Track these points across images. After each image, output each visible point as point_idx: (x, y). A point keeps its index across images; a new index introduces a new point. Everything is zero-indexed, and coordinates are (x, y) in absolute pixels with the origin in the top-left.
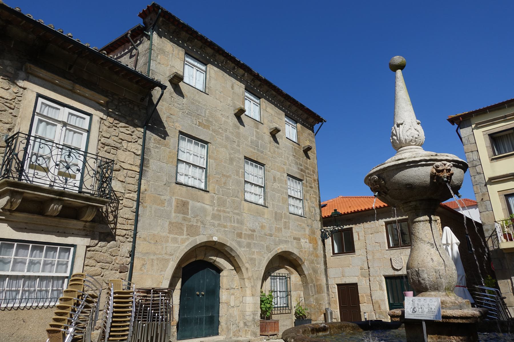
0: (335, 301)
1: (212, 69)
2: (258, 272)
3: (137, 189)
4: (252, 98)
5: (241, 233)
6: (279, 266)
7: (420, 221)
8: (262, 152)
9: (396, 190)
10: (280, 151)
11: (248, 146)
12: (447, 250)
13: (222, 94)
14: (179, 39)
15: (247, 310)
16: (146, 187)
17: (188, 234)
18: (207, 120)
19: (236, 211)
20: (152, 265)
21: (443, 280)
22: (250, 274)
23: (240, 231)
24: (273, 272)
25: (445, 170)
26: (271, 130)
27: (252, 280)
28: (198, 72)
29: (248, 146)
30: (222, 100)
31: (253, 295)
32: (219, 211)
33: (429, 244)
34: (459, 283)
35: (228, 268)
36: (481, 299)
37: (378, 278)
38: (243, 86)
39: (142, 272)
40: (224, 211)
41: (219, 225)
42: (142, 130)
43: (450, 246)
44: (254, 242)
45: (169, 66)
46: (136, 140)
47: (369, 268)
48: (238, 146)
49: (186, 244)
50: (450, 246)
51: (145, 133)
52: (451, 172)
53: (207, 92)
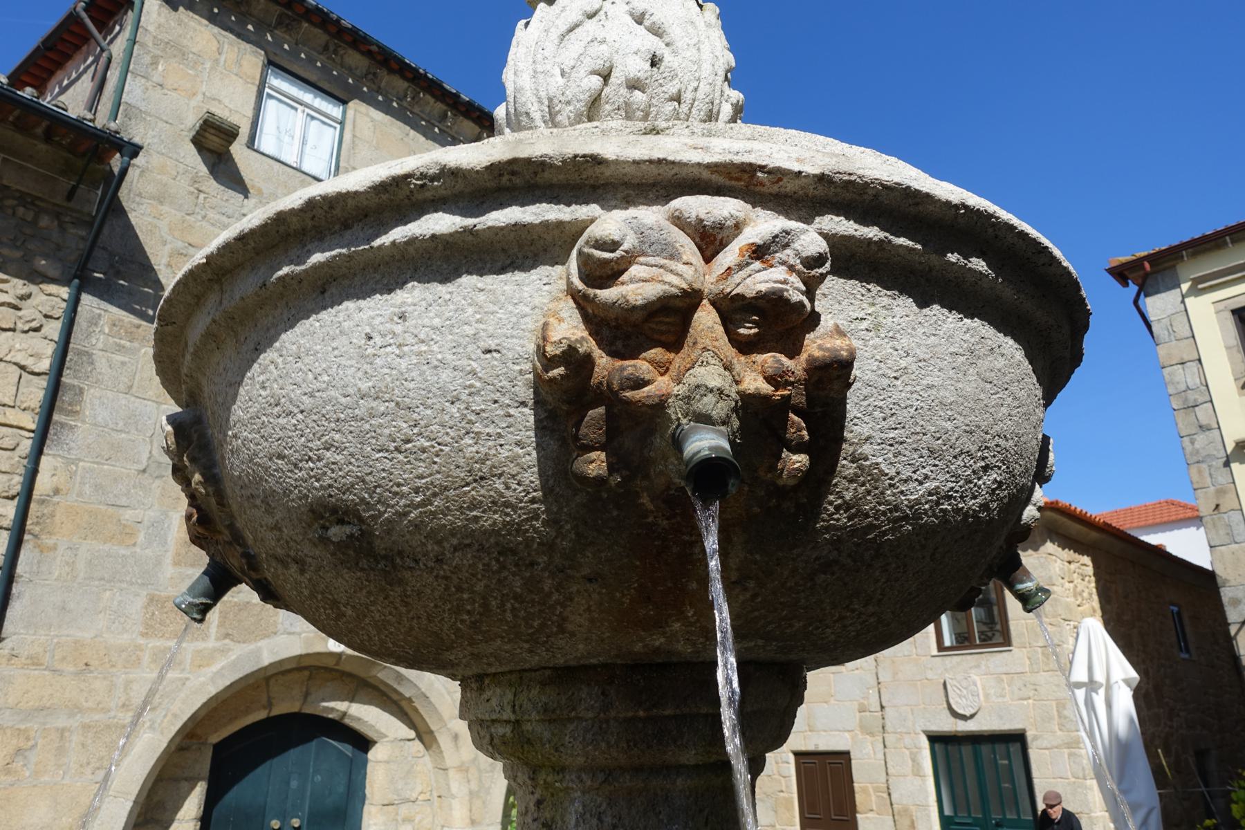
0: (790, 801)
3: (18, 488)
12: (1090, 704)
14: (244, 17)
16: (61, 480)
17: (227, 636)
20: (61, 751)
25: (706, 319)
28: (315, 123)
39: (10, 779)
42: (64, 292)
43: (1102, 691)
45: (200, 97)
46: (34, 324)
47: (882, 707)
49: (215, 668)
50: (1102, 691)
51: (75, 303)
52: (816, 345)
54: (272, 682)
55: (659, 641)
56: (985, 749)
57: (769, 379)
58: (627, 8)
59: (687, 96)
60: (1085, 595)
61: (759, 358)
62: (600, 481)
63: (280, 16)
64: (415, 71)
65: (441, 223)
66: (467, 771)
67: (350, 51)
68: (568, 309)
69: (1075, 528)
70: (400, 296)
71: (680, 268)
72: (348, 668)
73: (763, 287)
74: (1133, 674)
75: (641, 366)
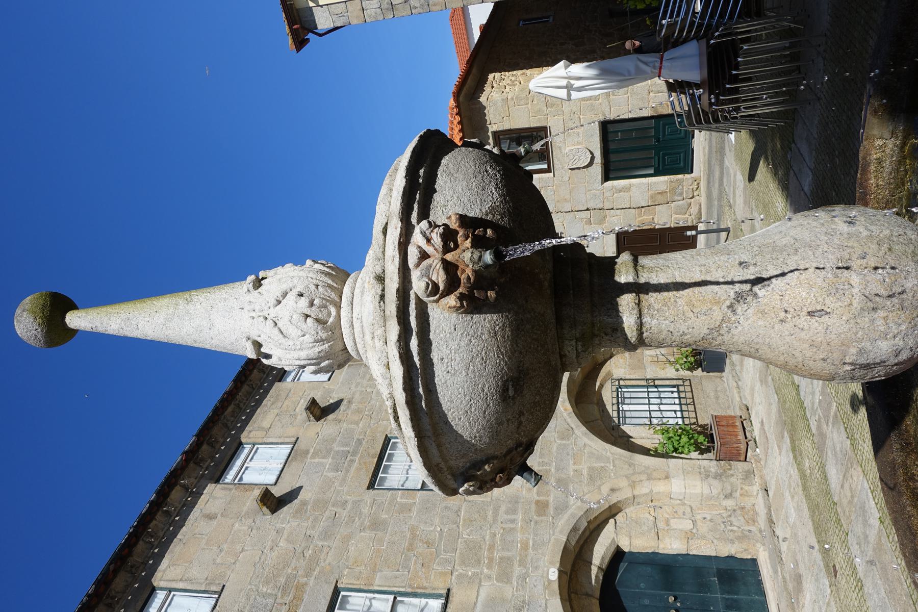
1: (167, 572)
2: (617, 462)
4: (238, 463)
5: (537, 502)
6: (598, 404)
7: (640, 326)
8: (359, 442)
9: (520, 423)
10: (357, 396)
11: (344, 480)
13: (225, 547)
15: (698, 490)
18: (285, 590)
19: (490, 513)
21: (909, 285)
22: (623, 483)
23: (533, 506)
24: (610, 418)
25: (449, 257)
26: (312, 418)
27: (636, 478)
29: (344, 480)
30: (238, 547)
31: (667, 477)
32: (491, 560)
33: (740, 309)
34: (654, 67)
35: (613, 535)
36: (692, 23)
37: (608, 194)
38: (210, 487)
40: (492, 547)
41: (522, 563)
43: (572, 82)
44: (553, 470)
48: (344, 504)
50: (572, 82)
52: (454, 224)
53: (219, 589)
55: (546, 284)
56: (612, 146)
57: (467, 239)
58: (272, 308)
59: (315, 281)
60: (513, 79)
61: (459, 242)
62: (496, 293)
64: (131, 535)
65: (414, 344)
66: (634, 482)
67: (113, 586)
68: (444, 301)
69: (470, 82)
70: (435, 361)
71: (434, 264)
72: (569, 567)
73: (440, 240)
74: (562, 63)
75: (463, 278)
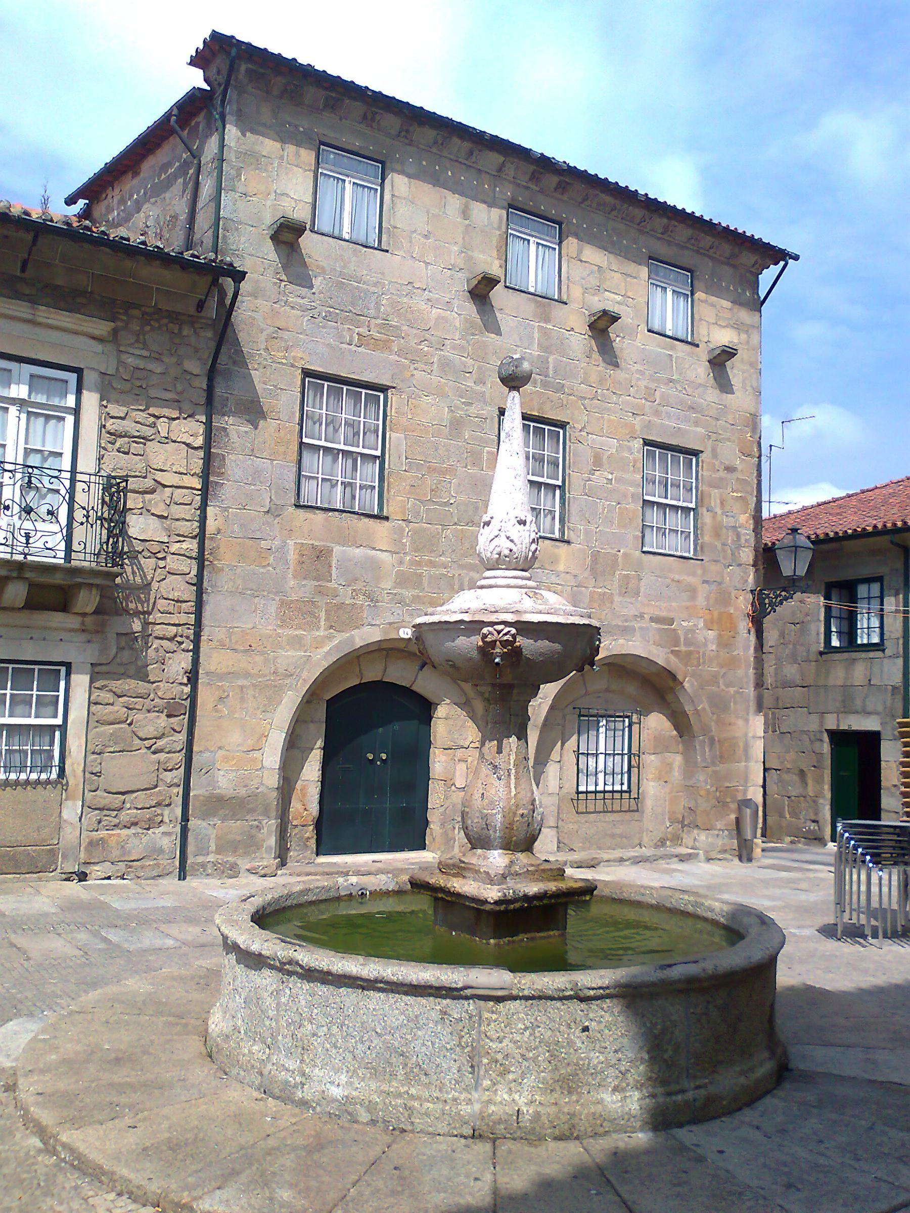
16: (219, 523)
17: (331, 627)
20: (242, 700)
45: (273, 196)
54: (361, 659)
63: (326, 99)
